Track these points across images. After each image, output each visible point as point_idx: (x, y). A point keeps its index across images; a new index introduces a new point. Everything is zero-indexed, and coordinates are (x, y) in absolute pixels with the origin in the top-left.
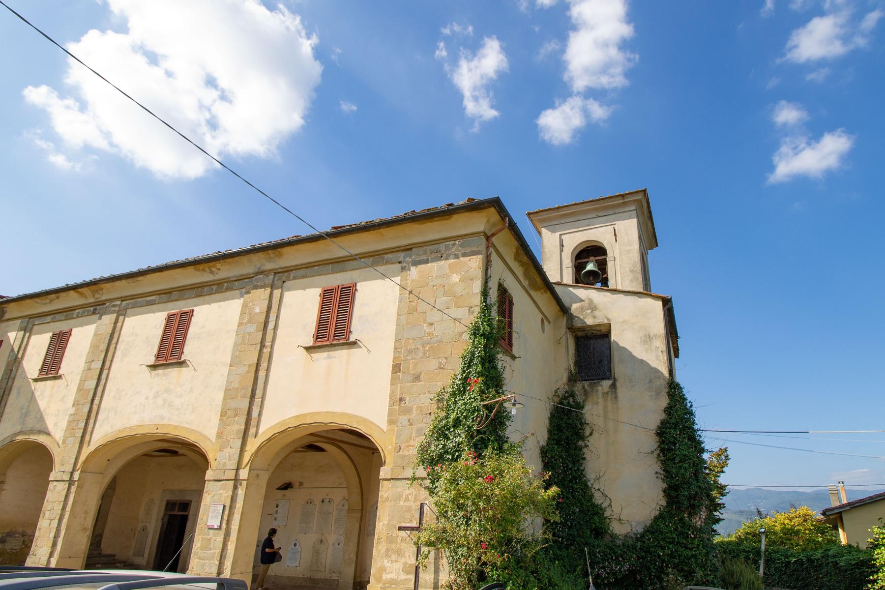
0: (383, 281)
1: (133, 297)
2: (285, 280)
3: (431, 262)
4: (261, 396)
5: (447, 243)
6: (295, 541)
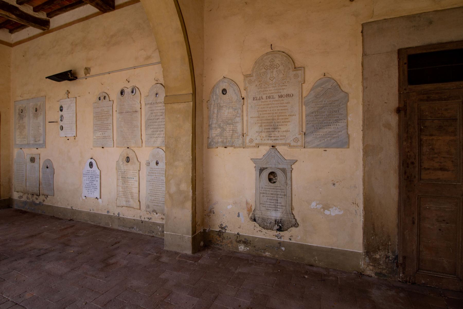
6: (90, 160)
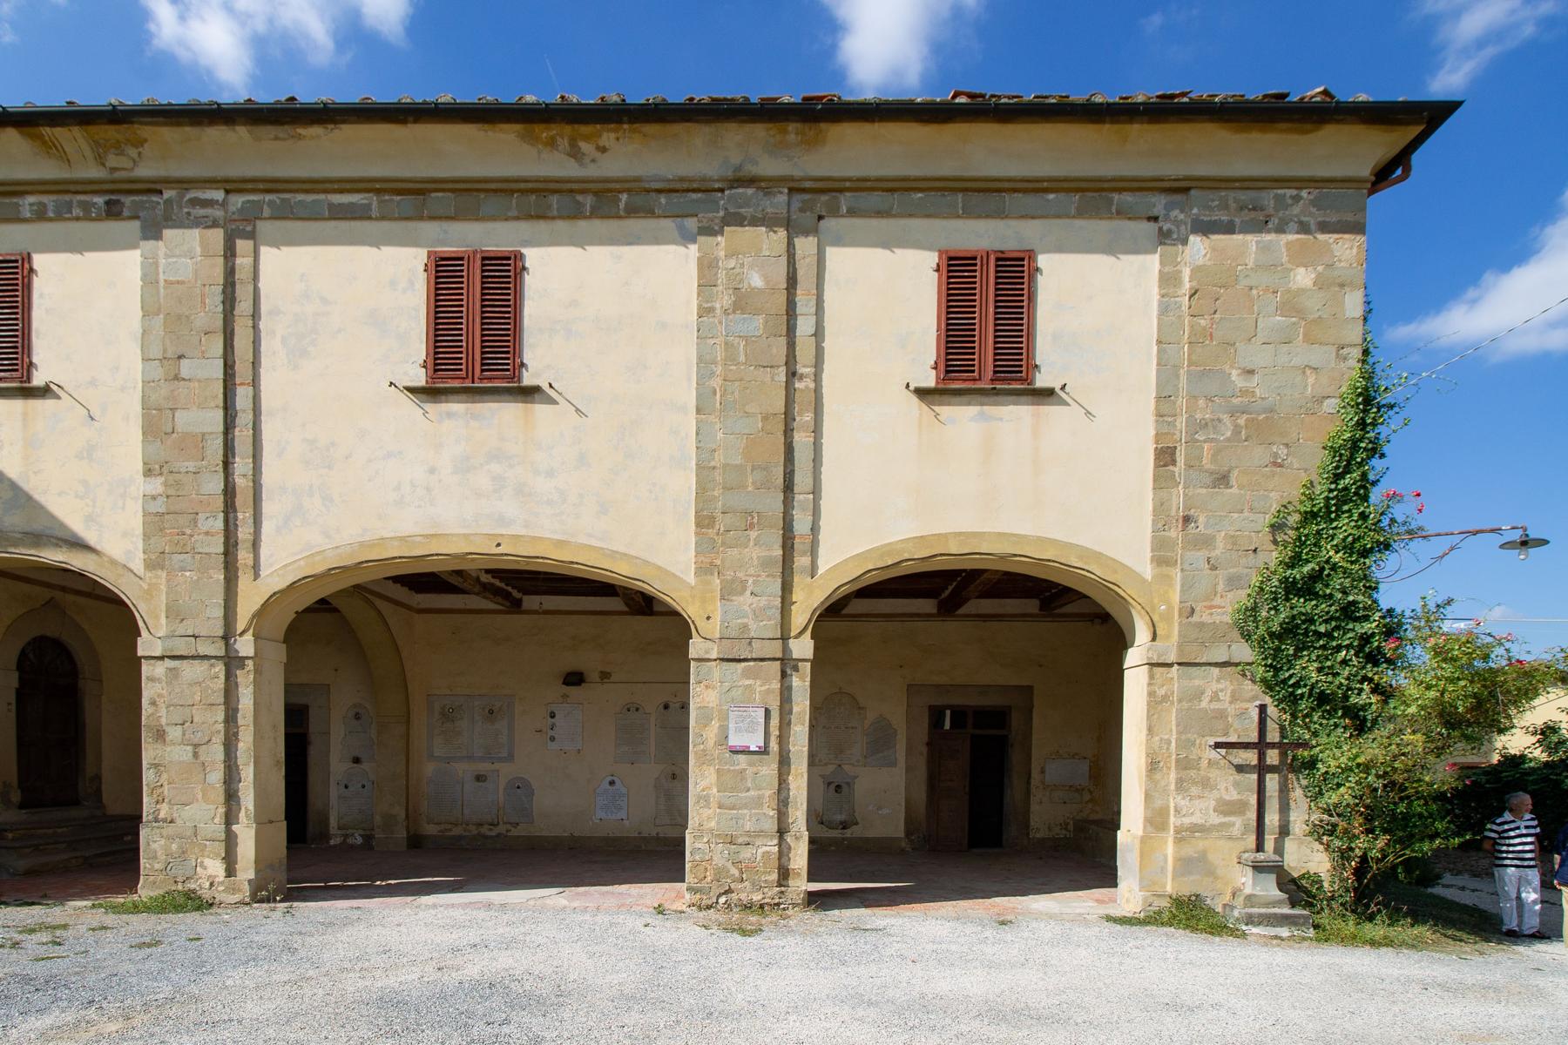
0: (80, 256)
1: (272, 185)
2: (824, 213)
3: (1240, 233)
4: (810, 487)
5: (1279, 191)
